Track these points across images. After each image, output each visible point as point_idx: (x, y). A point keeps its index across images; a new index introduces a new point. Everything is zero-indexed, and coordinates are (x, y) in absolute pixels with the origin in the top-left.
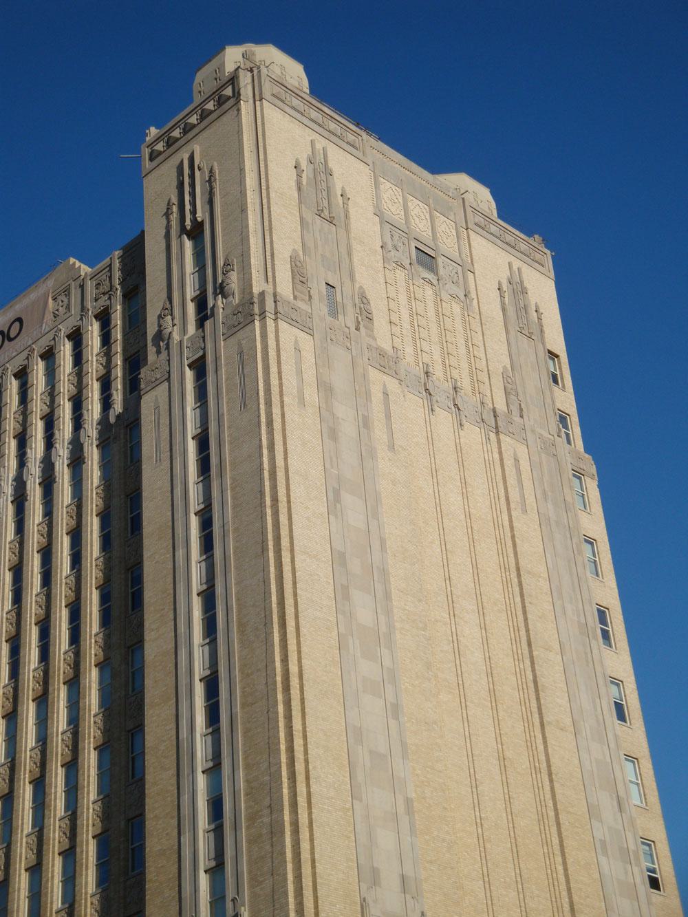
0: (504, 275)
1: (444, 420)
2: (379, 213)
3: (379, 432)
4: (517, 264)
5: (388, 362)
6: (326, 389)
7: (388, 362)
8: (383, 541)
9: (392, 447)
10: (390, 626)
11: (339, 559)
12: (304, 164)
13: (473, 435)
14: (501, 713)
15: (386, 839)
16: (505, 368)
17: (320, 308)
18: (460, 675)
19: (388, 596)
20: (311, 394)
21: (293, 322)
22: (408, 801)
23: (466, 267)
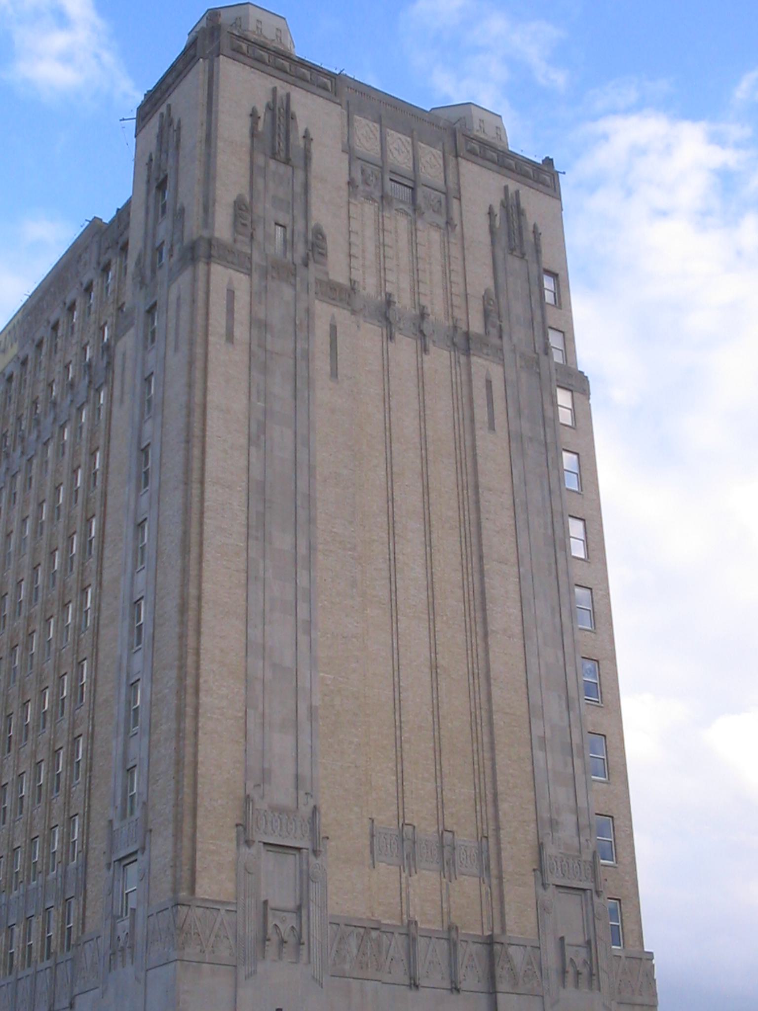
0: (496, 200)
4: (513, 186)
5: (343, 294)
7: (343, 294)
8: (311, 468)
9: (334, 373)
10: (311, 548)
12: (261, 111)
13: (440, 359)
19: (311, 521)
20: (241, 331)
21: (228, 263)
22: (312, 712)
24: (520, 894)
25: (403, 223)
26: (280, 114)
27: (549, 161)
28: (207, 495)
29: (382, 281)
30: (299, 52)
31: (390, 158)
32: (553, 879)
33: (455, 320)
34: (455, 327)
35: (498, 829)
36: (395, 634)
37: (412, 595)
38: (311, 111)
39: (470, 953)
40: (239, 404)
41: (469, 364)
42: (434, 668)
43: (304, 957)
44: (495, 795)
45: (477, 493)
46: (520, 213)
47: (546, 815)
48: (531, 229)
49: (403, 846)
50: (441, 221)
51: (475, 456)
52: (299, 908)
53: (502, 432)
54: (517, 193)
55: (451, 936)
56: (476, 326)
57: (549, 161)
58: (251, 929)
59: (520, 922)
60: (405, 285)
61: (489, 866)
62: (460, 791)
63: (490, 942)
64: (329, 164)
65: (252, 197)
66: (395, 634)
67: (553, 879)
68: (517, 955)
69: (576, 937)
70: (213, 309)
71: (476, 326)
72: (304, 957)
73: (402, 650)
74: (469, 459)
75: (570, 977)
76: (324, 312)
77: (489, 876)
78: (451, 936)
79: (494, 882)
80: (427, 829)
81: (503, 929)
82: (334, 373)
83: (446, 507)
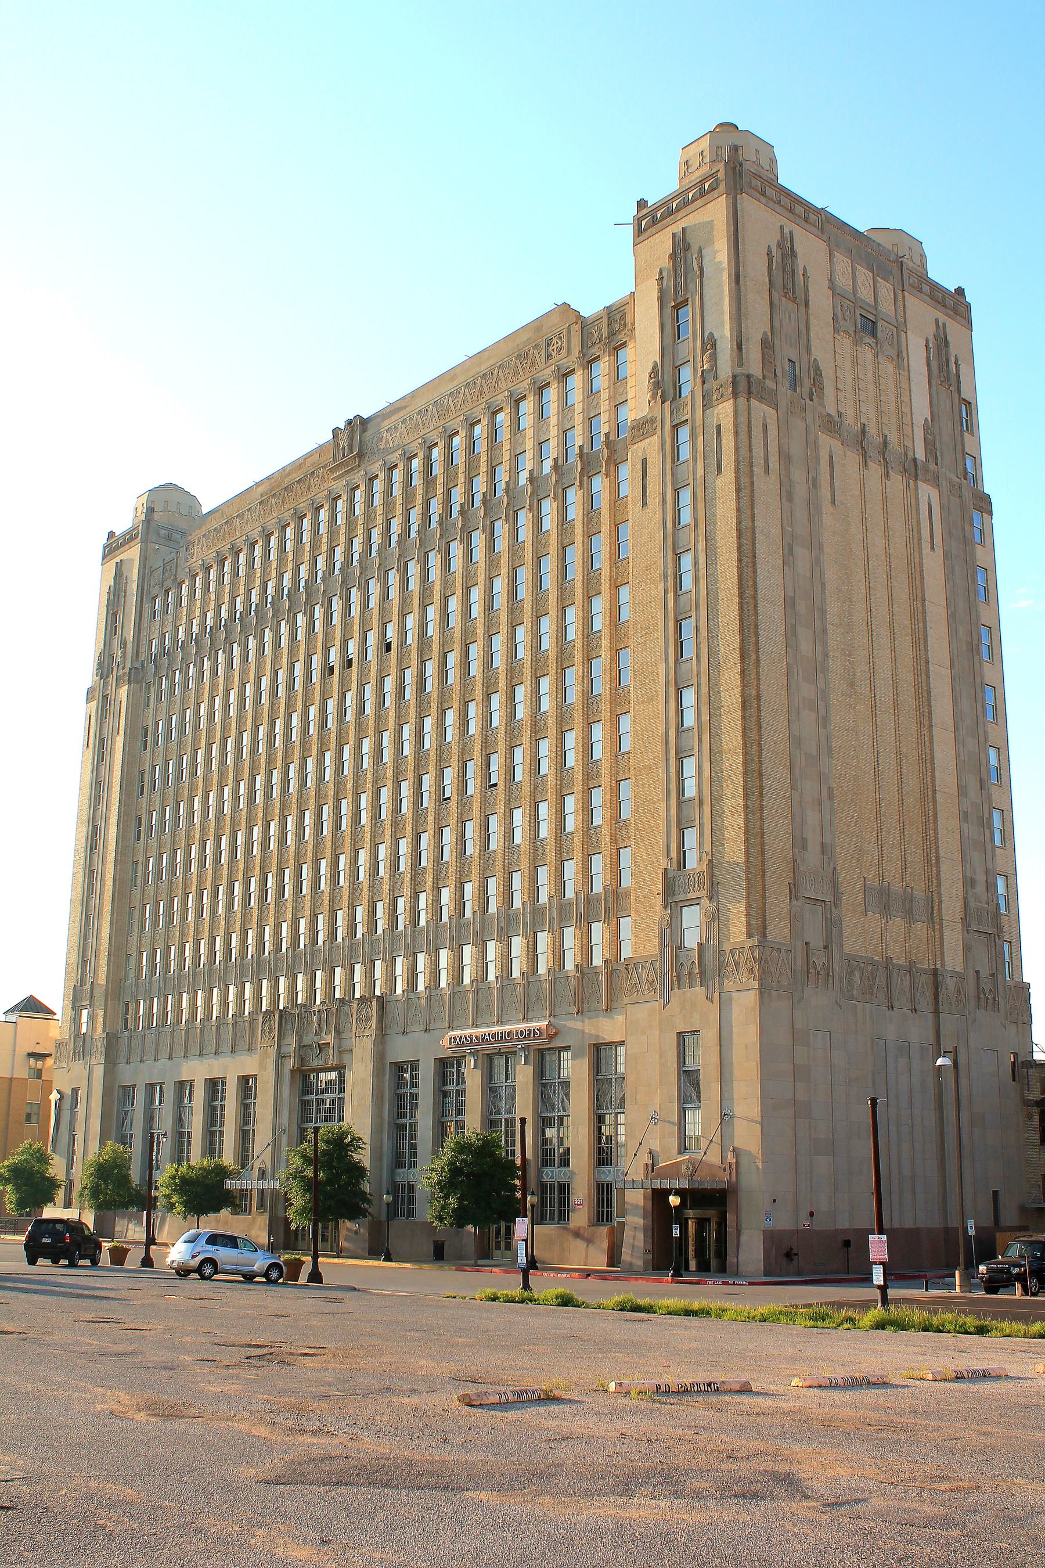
1: (875, 469)
2: (832, 285)
3: (825, 492)
4: (942, 318)
5: (833, 425)
6: (785, 457)
7: (833, 425)
8: (823, 585)
9: (833, 502)
10: (825, 655)
11: (790, 603)
14: (901, 718)
15: (812, 818)
16: (765, 333)
17: (784, 390)
18: (873, 690)
20: (774, 463)
21: (761, 399)
22: (830, 791)
23: (901, 327)
24: (953, 936)
25: (869, 355)
26: (788, 251)
27: (960, 291)
28: (760, 610)
29: (858, 413)
30: (783, 180)
31: (859, 294)
32: (974, 926)
33: (906, 448)
34: (906, 454)
35: (939, 885)
36: (875, 725)
37: (885, 696)
38: (810, 250)
39: (925, 979)
40: (776, 531)
41: (916, 488)
42: (899, 753)
43: (831, 986)
44: (938, 858)
45: (923, 605)
46: (793, 253)
47: (968, 875)
48: (801, 273)
49: (883, 900)
50: (893, 352)
51: (922, 571)
52: (826, 947)
53: (939, 551)
54: (944, 325)
55: (911, 968)
56: (920, 454)
57: (960, 291)
58: (800, 964)
59: (953, 961)
60: (872, 416)
61: (933, 915)
62: (916, 857)
63: (935, 973)
64: (821, 300)
65: (772, 334)
66: (875, 725)
67: (974, 926)
68: (950, 983)
69: (985, 972)
70: (754, 441)
71: (920, 454)
72: (831, 986)
73: (879, 739)
74: (918, 574)
75: (982, 1003)
76: (827, 443)
77: (933, 923)
78: (911, 968)
79: (937, 927)
80: (897, 886)
81: (943, 965)
82: (833, 502)
83: (904, 620)
